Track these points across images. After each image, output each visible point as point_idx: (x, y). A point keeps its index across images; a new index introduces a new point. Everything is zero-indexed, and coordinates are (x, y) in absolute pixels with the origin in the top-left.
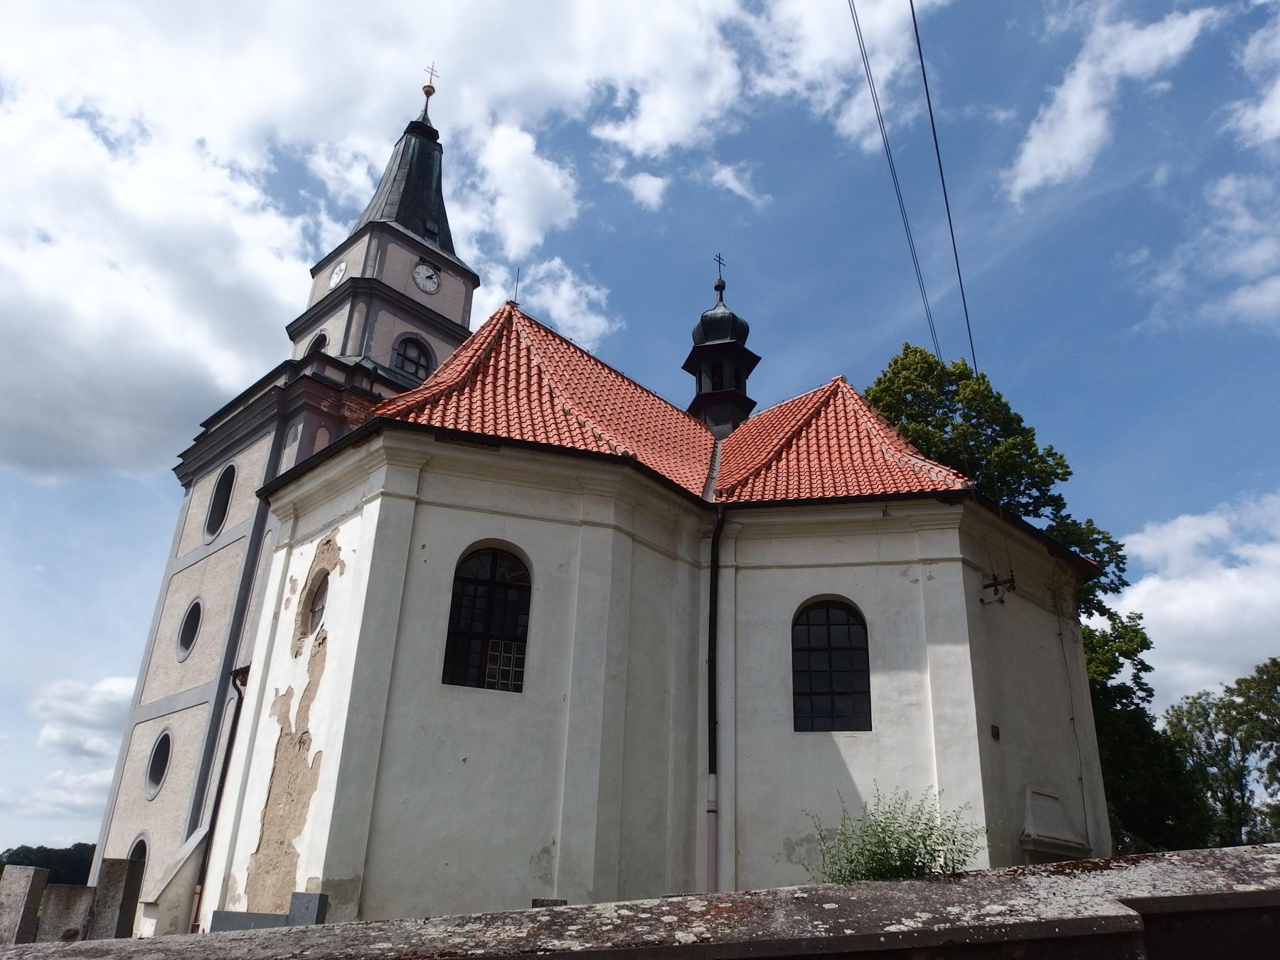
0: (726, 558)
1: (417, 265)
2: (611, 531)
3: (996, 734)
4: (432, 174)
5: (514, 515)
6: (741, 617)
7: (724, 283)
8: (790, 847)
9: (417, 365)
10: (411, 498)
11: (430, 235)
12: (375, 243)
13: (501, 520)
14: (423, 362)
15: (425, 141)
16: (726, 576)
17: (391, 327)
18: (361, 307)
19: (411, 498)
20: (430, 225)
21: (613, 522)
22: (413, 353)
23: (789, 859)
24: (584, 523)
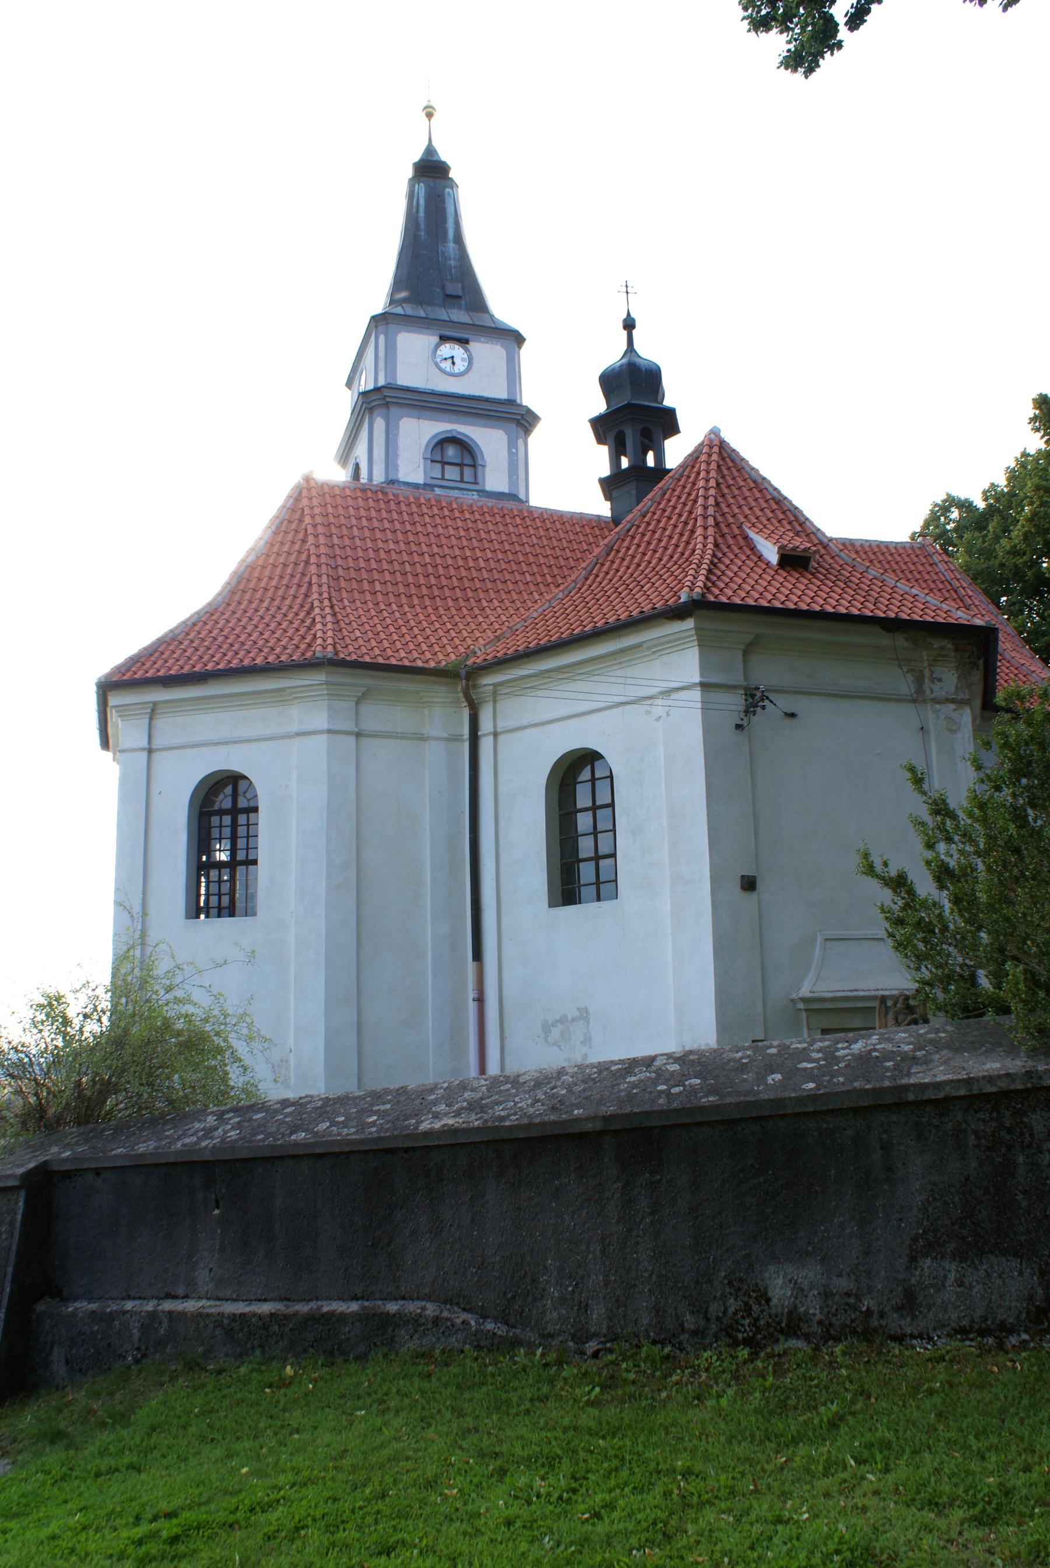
0: (486, 725)
1: (437, 346)
2: (325, 736)
3: (749, 884)
4: (444, 221)
5: (235, 742)
6: (502, 789)
7: (633, 320)
8: (547, 1028)
9: (461, 465)
10: (143, 749)
11: (452, 299)
12: (382, 339)
13: (223, 750)
14: (468, 461)
15: (431, 181)
16: (486, 745)
17: (417, 433)
18: (380, 423)
19: (143, 749)
20: (453, 288)
21: (325, 727)
22: (451, 452)
23: (547, 1042)
24: (298, 734)
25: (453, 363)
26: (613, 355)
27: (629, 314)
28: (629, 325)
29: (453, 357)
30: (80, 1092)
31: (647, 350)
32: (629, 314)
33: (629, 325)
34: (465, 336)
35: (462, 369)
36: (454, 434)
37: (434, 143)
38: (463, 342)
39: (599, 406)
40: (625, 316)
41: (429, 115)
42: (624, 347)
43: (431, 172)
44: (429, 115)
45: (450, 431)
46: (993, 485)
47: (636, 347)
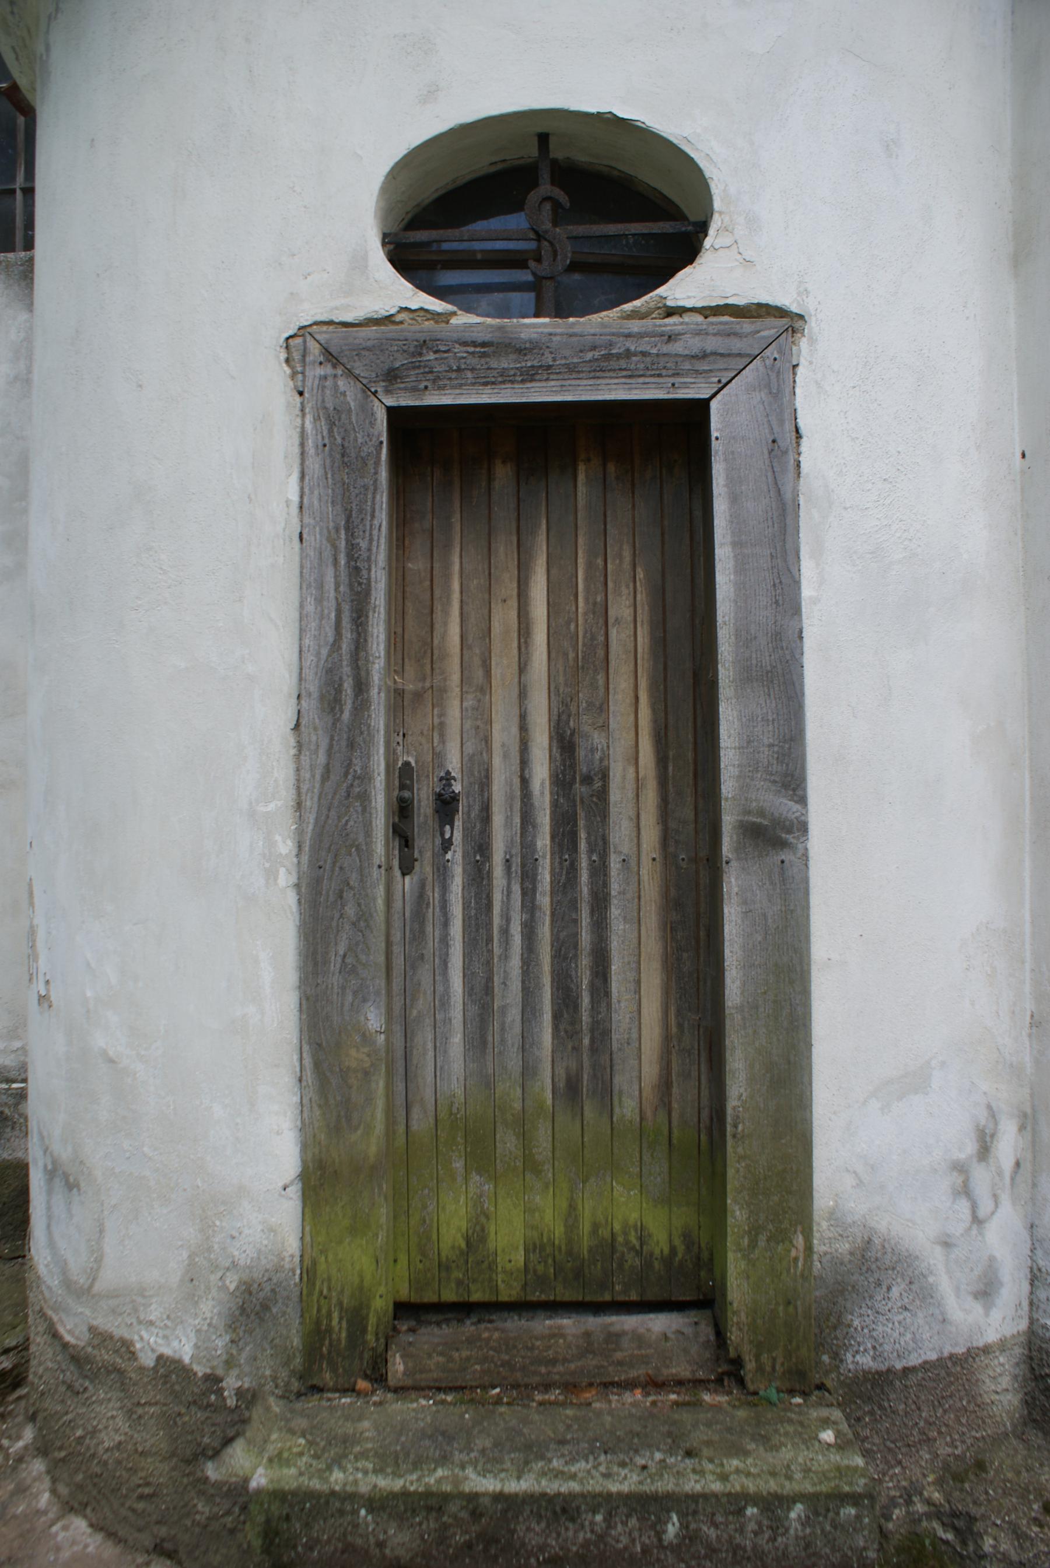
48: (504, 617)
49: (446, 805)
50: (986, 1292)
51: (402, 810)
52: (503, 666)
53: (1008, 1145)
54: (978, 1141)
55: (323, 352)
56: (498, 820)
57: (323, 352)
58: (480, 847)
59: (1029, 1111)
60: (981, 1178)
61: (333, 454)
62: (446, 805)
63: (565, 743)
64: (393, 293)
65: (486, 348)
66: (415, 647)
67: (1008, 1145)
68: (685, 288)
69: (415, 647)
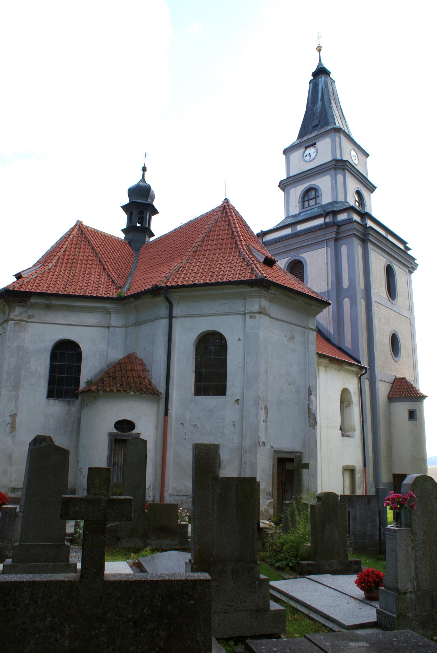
25: (310, 156)
26: (135, 181)
27: (145, 165)
28: (144, 169)
29: (310, 154)
30: (9, 307)
31: (149, 181)
32: (145, 165)
33: (144, 169)
34: (314, 142)
35: (306, 159)
36: (309, 187)
37: (322, 62)
38: (314, 145)
39: (126, 201)
40: (143, 166)
41: (319, 51)
42: (141, 178)
43: (321, 72)
44: (319, 51)
45: (308, 186)
46: (356, 582)
47: (145, 179)
48: (120, 451)
49: (116, 464)
50: (150, 497)
51: (113, 464)
52: (120, 455)
53: (152, 487)
54: (108, 366)
55: (110, 435)
56: (327, 625)
57: (110, 435)
58: (118, 466)
59: (409, 252)
60: (150, 489)
61: (110, 441)
62: (116, 464)
63: (124, 460)
64: (115, 431)
65: (121, 435)
66: (115, 453)
67: (152, 487)
68: (133, 432)
69: (115, 453)
